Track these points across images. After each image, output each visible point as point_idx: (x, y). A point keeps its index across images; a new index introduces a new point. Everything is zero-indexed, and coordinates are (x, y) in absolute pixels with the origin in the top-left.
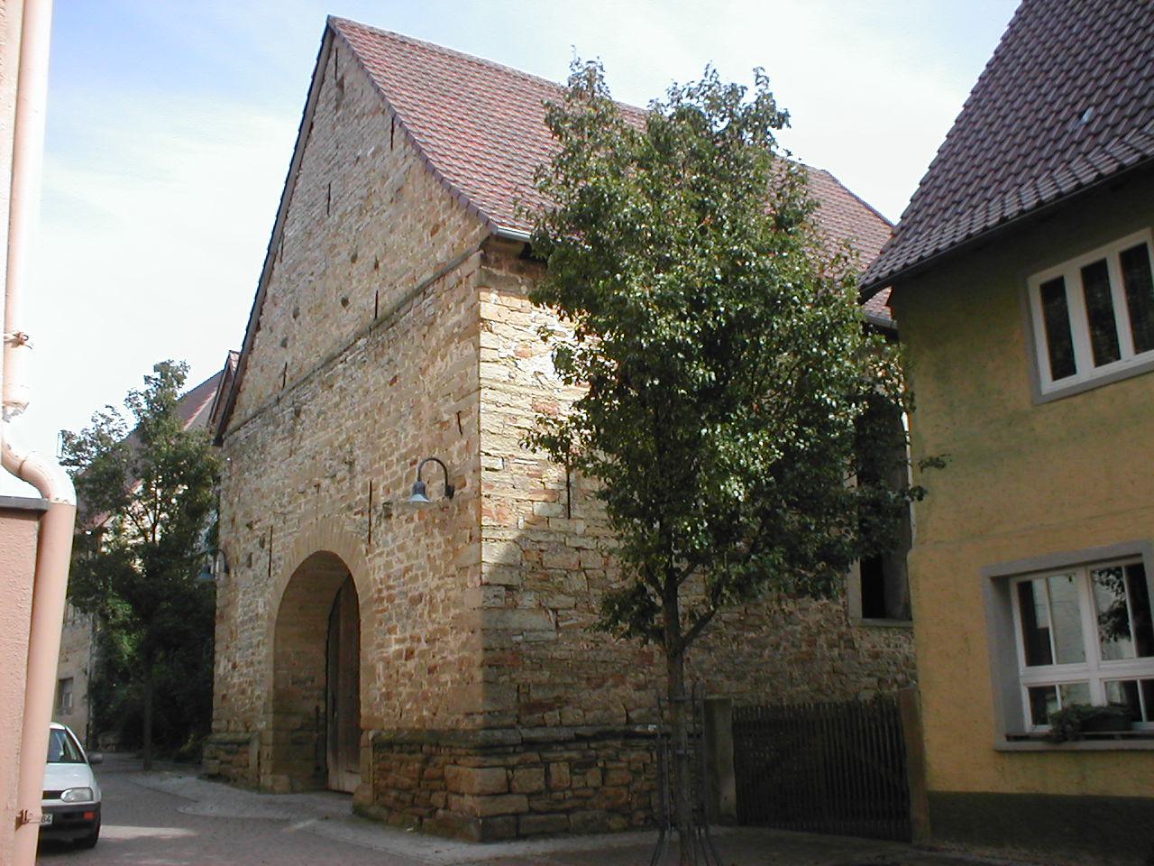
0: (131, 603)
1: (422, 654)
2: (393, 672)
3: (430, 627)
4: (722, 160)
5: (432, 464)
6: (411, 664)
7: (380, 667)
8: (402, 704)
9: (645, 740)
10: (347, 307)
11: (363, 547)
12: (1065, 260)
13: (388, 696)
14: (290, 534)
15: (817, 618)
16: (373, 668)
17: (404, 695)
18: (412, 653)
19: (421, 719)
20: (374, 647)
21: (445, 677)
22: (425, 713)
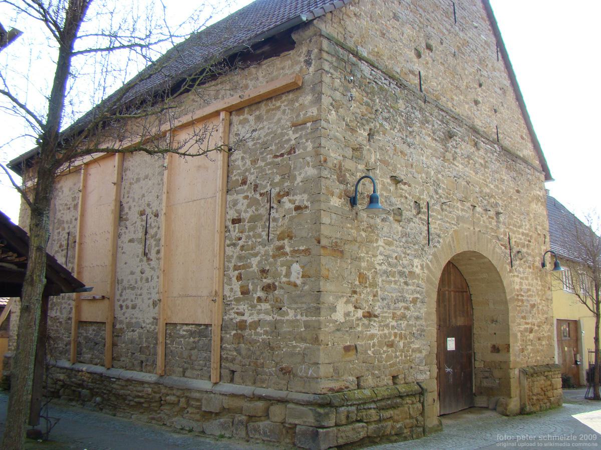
0: (69, 61)
1: (536, 331)
2: (525, 338)
3: (539, 320)
4: (452, 433)
5: (364, 184)
6: (532, 335)
7: (519, 334)
8: (529, 354)
9: (509, 82)
10: (434, 49)
11: (508, 268)
12: (209, 32)
13: (522, 350)
14: (450, 223)
15: (531, 215)
16: (516, 336)
17: (529, 350)
18: (532, 330)
19: (537, 361)
20: (516, 324)
21: (544, 343)
22: (538, 358)
